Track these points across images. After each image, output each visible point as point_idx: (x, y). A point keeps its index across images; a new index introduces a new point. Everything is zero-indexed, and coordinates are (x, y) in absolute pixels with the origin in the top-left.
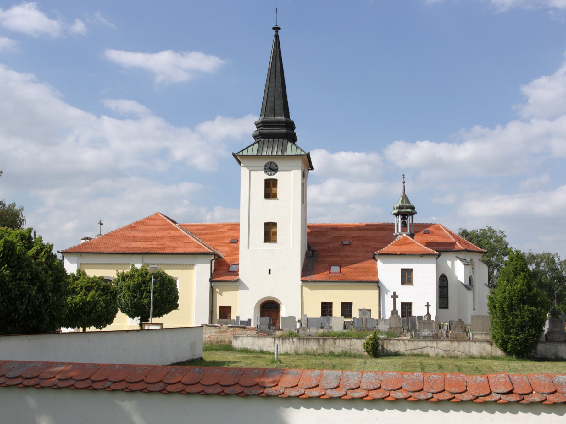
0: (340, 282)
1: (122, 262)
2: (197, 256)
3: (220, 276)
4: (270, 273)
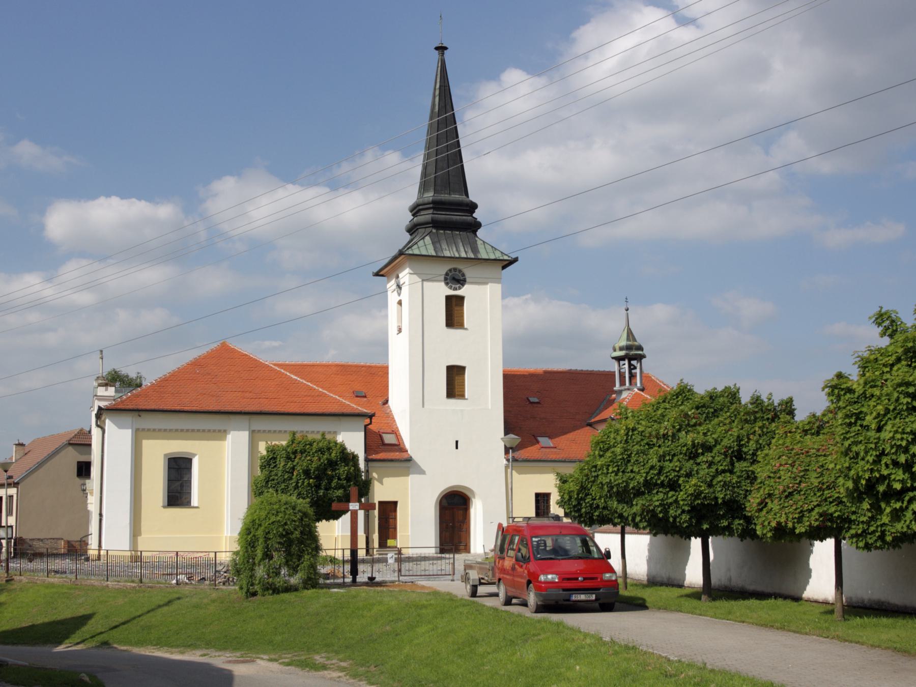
0: (565, 461)
1: (273, 429)
2: (232, 417)
3: (377, 453)
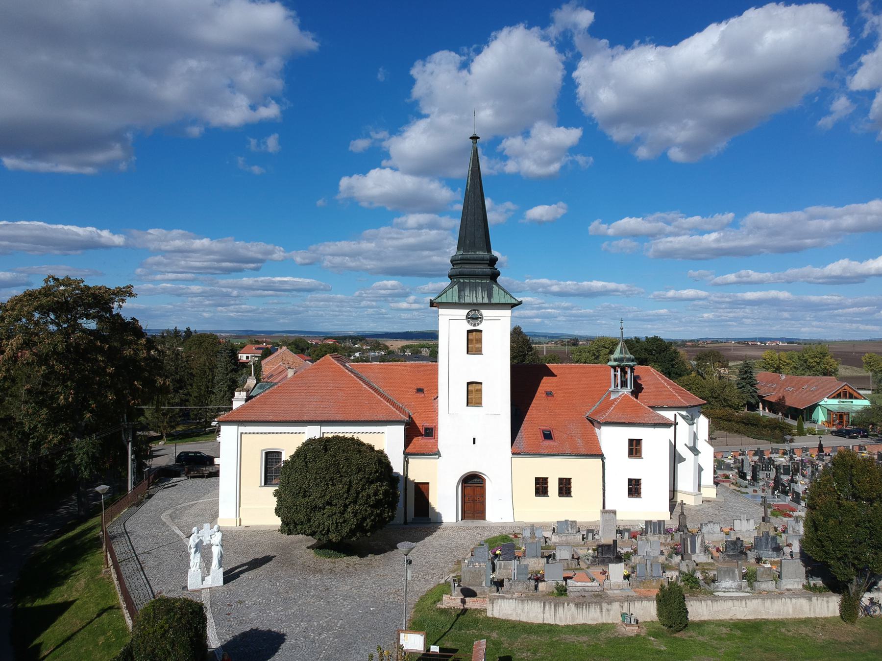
4: (474, 443)
